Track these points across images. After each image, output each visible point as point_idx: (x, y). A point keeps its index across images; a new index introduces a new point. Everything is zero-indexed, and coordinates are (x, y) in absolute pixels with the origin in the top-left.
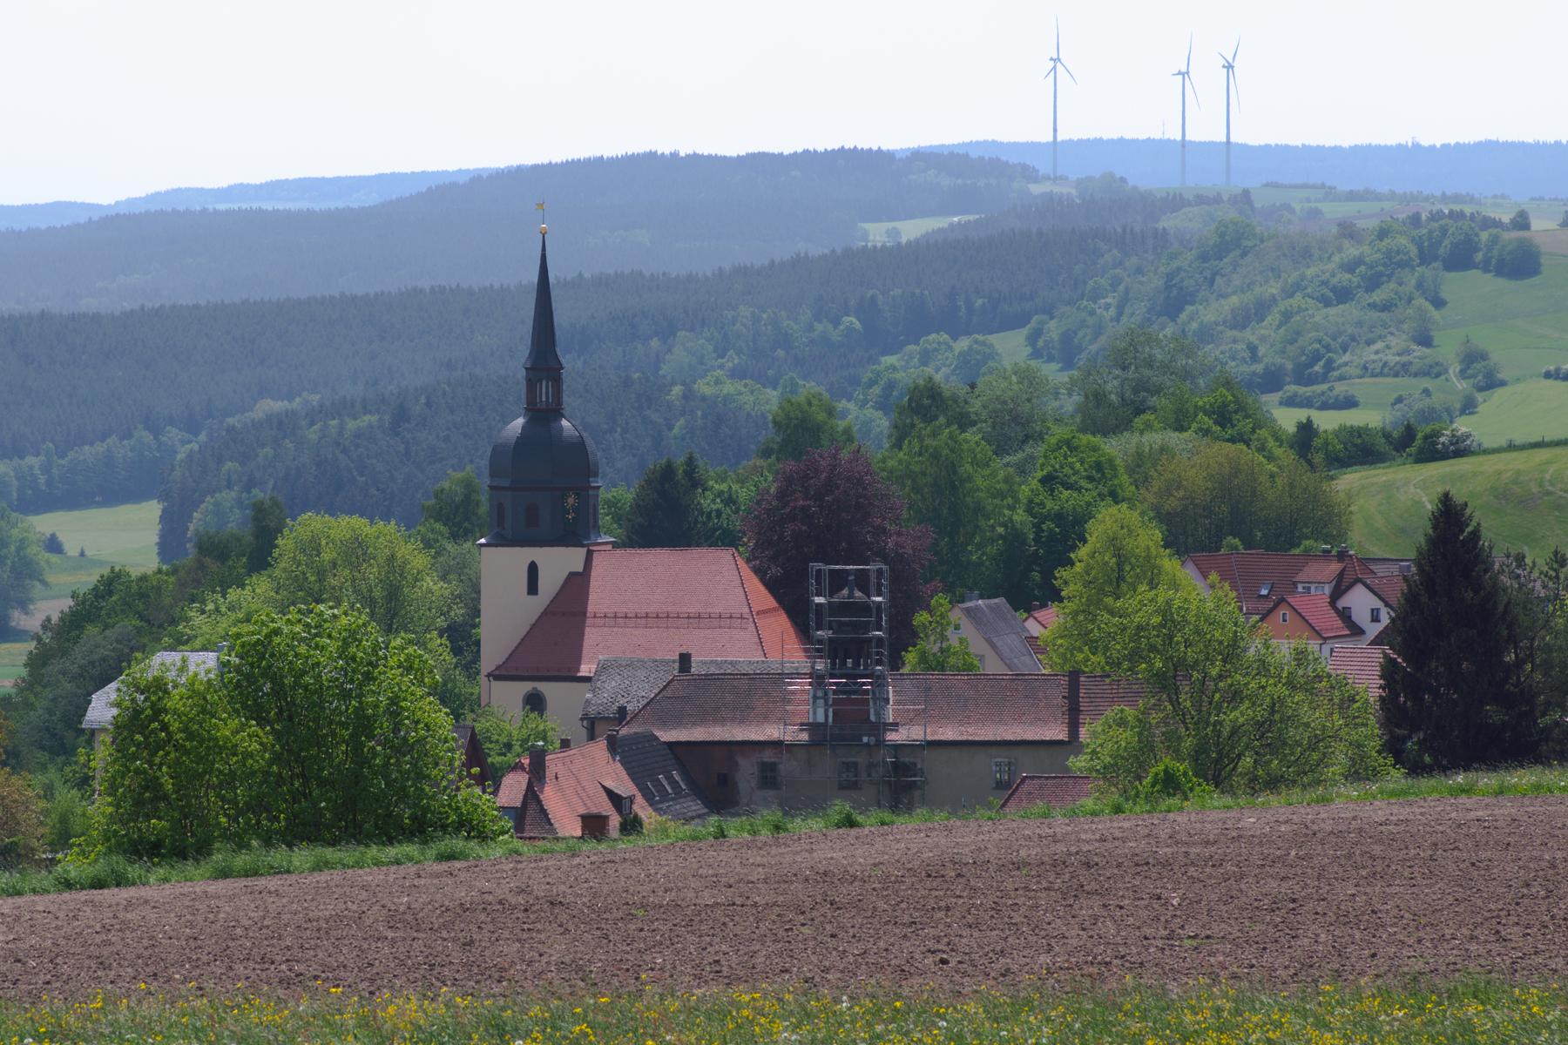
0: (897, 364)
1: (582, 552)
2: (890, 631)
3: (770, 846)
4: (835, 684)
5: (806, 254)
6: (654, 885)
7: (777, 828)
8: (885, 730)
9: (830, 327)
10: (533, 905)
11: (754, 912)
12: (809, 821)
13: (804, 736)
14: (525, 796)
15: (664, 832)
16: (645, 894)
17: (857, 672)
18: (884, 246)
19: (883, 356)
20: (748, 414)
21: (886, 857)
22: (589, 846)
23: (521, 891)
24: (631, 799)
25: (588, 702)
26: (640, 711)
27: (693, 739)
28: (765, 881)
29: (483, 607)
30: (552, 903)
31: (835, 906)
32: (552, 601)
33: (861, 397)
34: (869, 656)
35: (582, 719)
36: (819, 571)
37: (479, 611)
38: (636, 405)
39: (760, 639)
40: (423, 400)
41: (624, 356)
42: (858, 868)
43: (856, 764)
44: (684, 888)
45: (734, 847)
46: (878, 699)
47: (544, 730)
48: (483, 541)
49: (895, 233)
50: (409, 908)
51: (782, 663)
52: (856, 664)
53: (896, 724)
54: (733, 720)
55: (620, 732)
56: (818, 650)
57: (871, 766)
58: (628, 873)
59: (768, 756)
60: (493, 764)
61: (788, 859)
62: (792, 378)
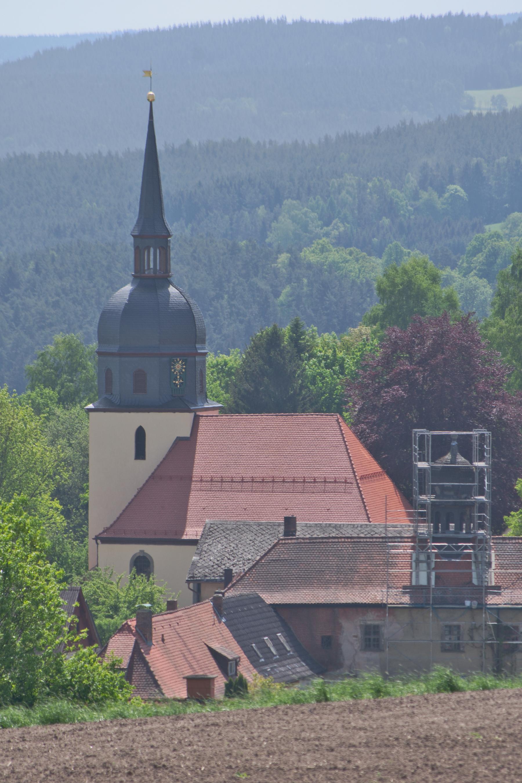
0: (500, 231)
1: (189, 417)
2: (493, 495)
3: (372, 709)
4: (439, 547)
5: (412, 122)
6: (257, 748)
7: (378, 692)
8: (487, 594)
9: (435, 195)
10: (137, 768)
11: (356, 776)
12: (410, 685)
13: (406, 599)
14: (132, 658)
15: (267, 694)
16: (248, 757)
17: (460, 536)
18: (489, 114)
19: (488, 224)
20: (354, 282)
21: (487, 722)
22: (193, 708)
23: (124, 754)
24: (237, 661)
25: (194, 564)
26: (246, 573)
27: (288, 602)
28: (367, 745)
29: (92, 471)
30: (155, 767)
31: (436, 771)
32: (159, 466)
33: (465, 265)
34: (471, 519)
35: (188, 582)
36: (422, 437)
37: (87, 476)
38: (244, 272)
39: (364, 503)
40: (32, 265)
41: (231, 224)
42: (460, 732)
43: (458, 627)
44: (286, 751)
45: (336, 710)
46: (481, 563)
47: (151, 593)
48: (91, 406)
49: (500, 100)
50: (13, 772)
51: (386, 527)
52: (459, 528)
53: (499, 588)
54: (337, 582)
55: (226, 595)
56: (422, 514)
57: (474, 629)
58: (231, 735)
59: (371, 618)
60: (100, 626)
61: (389, 723)
62: (396, 246)
